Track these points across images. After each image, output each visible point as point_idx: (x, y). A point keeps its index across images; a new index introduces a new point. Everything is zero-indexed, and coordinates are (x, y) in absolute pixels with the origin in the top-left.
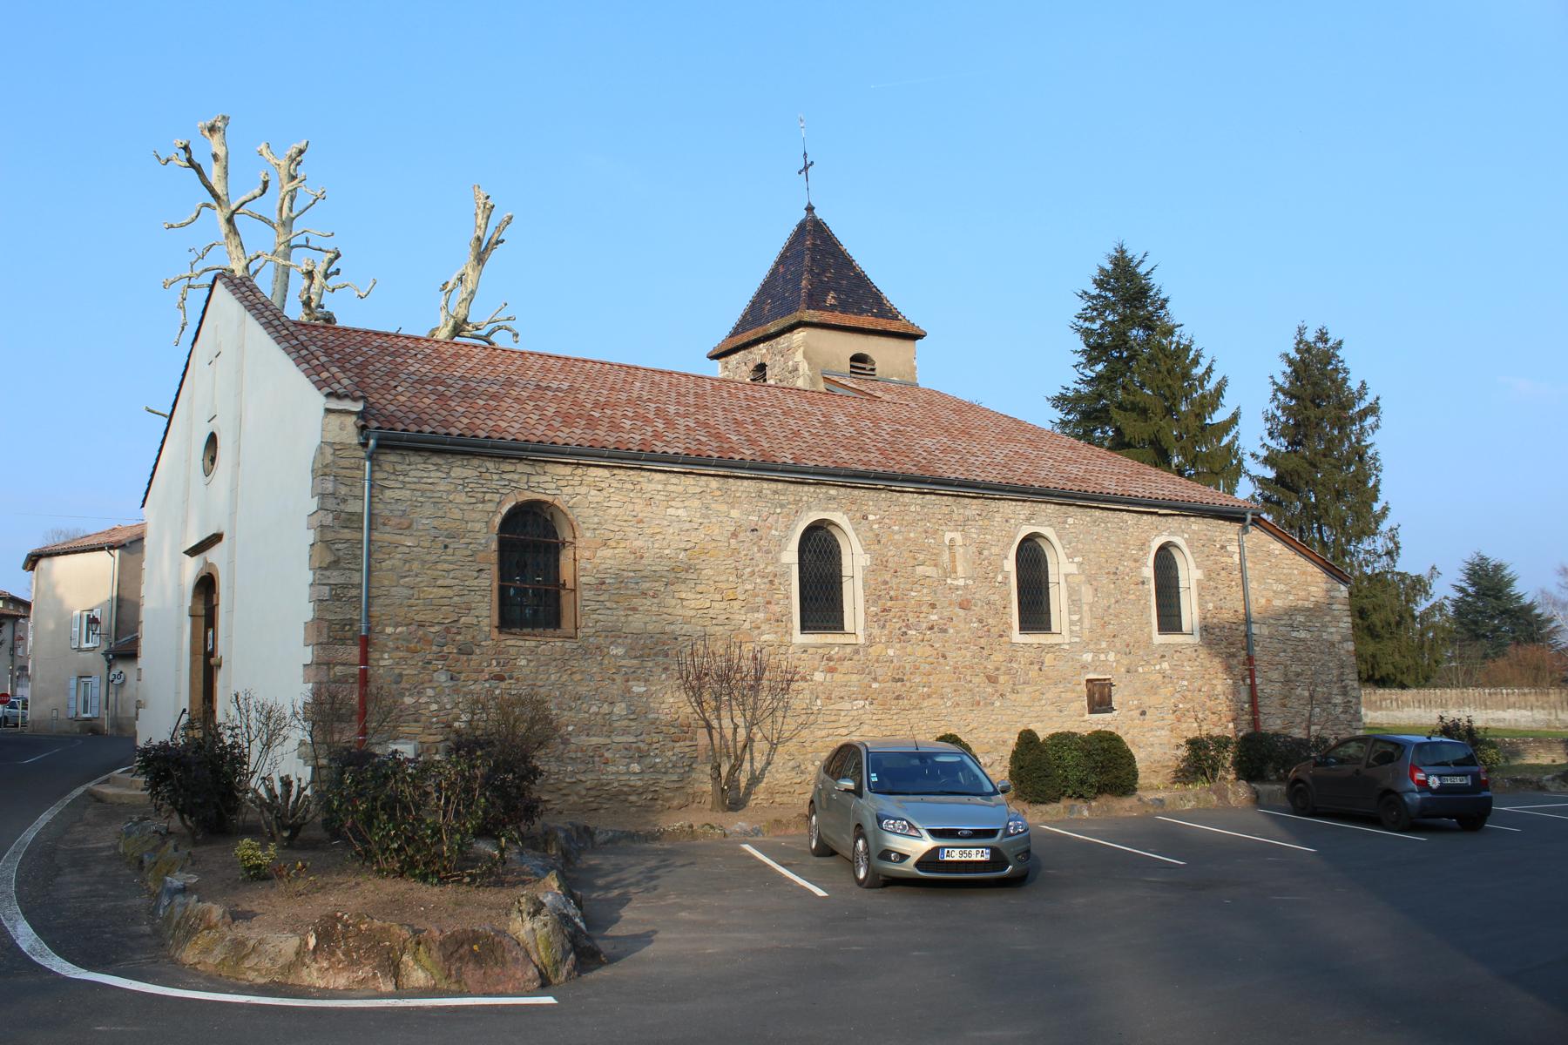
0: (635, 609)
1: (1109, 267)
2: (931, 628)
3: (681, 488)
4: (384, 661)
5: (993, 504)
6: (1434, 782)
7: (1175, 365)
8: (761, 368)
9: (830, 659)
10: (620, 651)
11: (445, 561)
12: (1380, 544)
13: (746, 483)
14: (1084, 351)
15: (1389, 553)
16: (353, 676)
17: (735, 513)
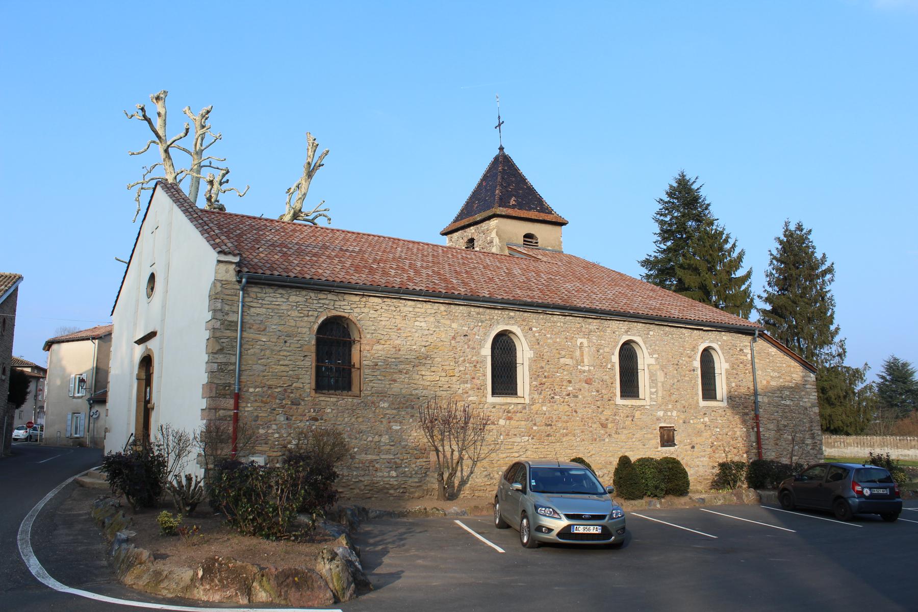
0: (395, 381)
1: (675, 185)
2: (568, 395)
4: (248, 408)
6: (867, 492)
8: (471, 241)
9: (509, 412)
10: (386, 405)
11: (285, 350)
12: (834, 349)
13: (461, 308)
15: (839, 355)
16: (230, 416)
17: (454, 325)
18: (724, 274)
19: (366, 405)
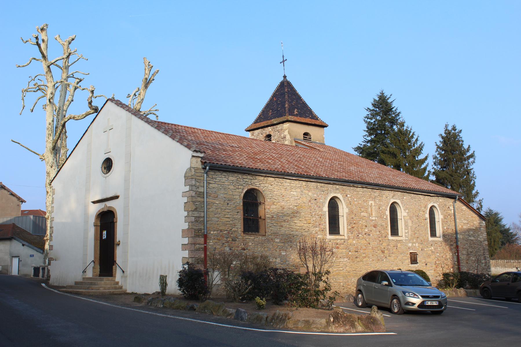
0: (282, 226)
1: (377, 99)
3: (294, 185)
4: (211, 243)
7: (404, 138)
8: (269, 136)
9: (337, 244)
10: (278, 240)
11: (228, 209)
13: (313, 183)
16: (202, 248)
17: (310, 194)
18: (411, 158)
19: (268, 240)
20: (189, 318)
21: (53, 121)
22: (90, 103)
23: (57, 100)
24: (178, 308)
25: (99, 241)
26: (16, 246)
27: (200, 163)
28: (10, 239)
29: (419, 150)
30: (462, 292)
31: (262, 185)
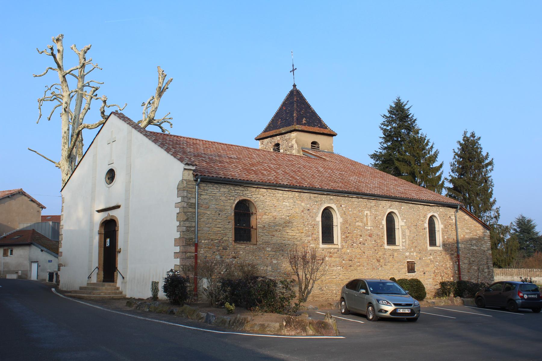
0: (274, 236)
1: (394, 106)
2: (360, 243)
4: (202, 251)
5: (379, 202)
6: (526, 296)
7: (418, 145)
8: (278, 145)
9: (330, 253)
10: (269, 249)
12: (493, 214)
13: (306, 194)
14: (384, 138)
15: (496, 217)
17: (303, 204)
18: (425, 166)
20: (165, 321)
21: (68, 130)
22: (103, 113)
23: (72, 108)
24: (160, 312)
25: (103, 249)
26: (35, 252)
27: (191, 175)
28: (29, 245)
29: (434, 158)
30: (458, 301)
31: (254, 196)
